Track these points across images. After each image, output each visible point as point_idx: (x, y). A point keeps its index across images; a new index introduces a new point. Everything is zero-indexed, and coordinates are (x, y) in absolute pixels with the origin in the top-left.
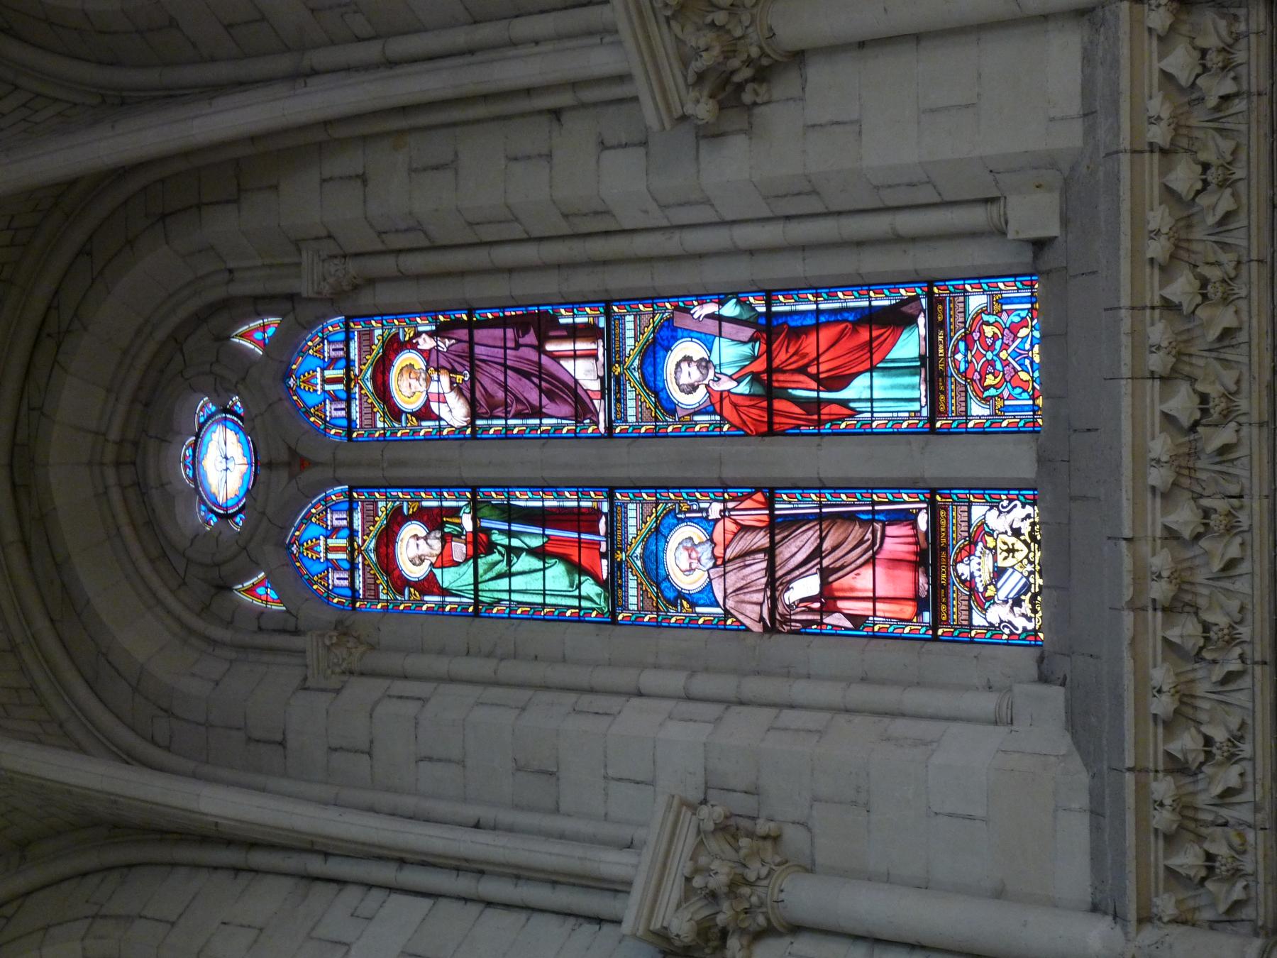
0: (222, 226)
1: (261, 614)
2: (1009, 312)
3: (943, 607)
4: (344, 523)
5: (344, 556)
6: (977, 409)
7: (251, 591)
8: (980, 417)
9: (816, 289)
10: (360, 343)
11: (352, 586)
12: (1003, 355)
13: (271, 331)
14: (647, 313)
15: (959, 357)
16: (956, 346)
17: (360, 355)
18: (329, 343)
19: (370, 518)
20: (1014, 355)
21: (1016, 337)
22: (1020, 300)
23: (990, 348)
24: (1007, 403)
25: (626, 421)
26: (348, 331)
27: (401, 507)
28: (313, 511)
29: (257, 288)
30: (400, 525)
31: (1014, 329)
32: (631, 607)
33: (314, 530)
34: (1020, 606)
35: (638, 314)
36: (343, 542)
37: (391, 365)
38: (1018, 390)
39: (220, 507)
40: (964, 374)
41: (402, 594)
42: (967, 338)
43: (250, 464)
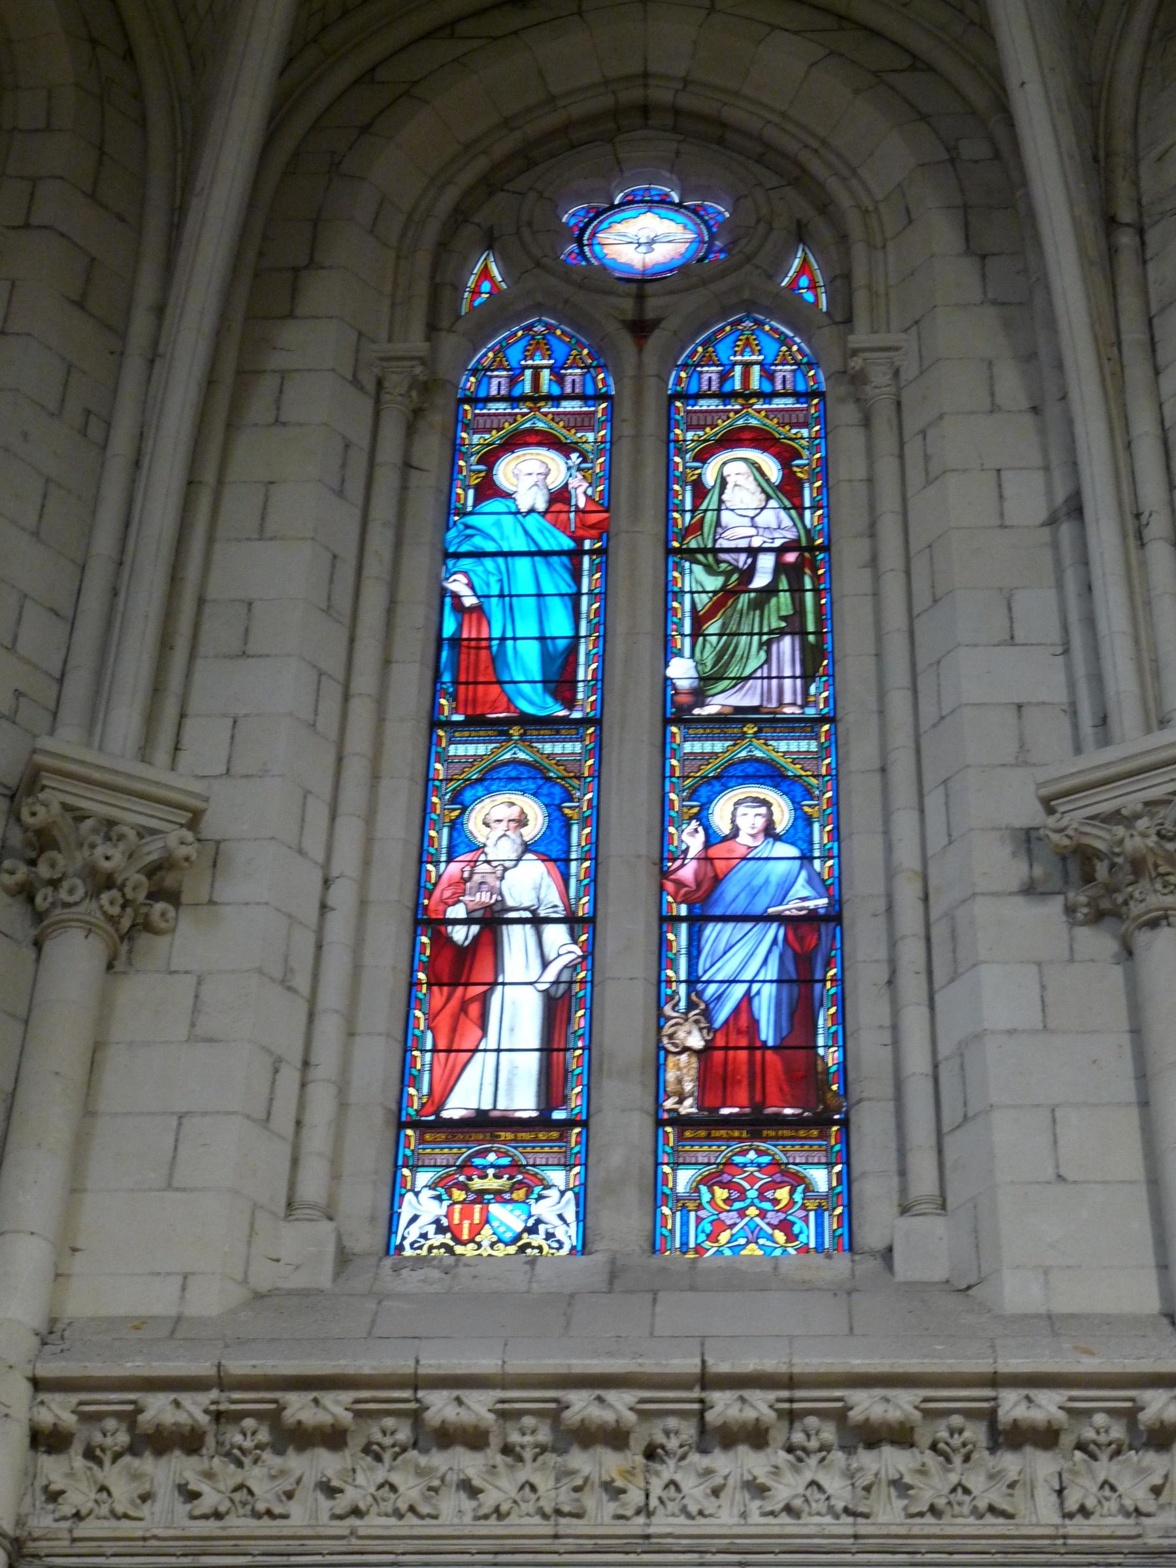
0: (940, 232)
1: (458, 288)
2: (806, 1220)
3: (703, 1133)
4: (779, 387)
5: (738, 386)
6: (684, 1179)
7: (485, 274)
8: (675, 1182)
9: (659, 982)
10: (579, 413)
11: (489, 399)
12: (753, 1211)
13: (809, 297)
14: (818, 767)
15: (752, 1155)
16: (506, 1154)
17: (564, 413)
18: (794, 371)
19: (788, 419)
20: (752, 1225)
21: (774, 1227)
22: (819, 1235)
23: (761, 1197)
24: (692, 1214)
25: (685, 740)
26: (599, 397)
27: (801, 457)
28: (795, 348)
29: (860, 277)
30: (777, 456)
31: (785, 1226)
32: (452, 747)
33: (771, 348)
34: (436, 1233)
35: (818, 757)
36: (755, 384)
37: (764, 449)
38: (708, 1229)
39: (593, 235)
40: (729, 1163)
41: (478, 463)
42: (515, 1166)
43: (643, 273)
